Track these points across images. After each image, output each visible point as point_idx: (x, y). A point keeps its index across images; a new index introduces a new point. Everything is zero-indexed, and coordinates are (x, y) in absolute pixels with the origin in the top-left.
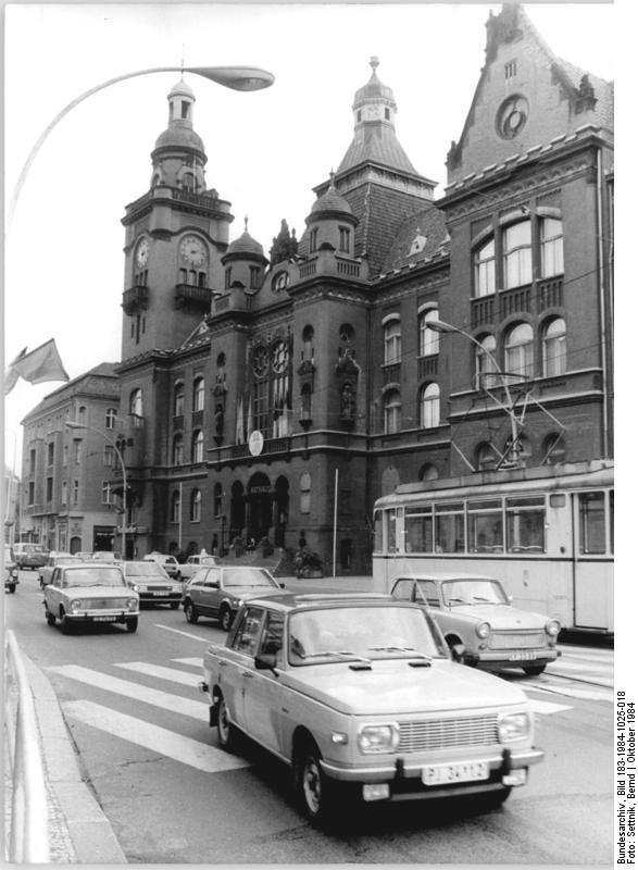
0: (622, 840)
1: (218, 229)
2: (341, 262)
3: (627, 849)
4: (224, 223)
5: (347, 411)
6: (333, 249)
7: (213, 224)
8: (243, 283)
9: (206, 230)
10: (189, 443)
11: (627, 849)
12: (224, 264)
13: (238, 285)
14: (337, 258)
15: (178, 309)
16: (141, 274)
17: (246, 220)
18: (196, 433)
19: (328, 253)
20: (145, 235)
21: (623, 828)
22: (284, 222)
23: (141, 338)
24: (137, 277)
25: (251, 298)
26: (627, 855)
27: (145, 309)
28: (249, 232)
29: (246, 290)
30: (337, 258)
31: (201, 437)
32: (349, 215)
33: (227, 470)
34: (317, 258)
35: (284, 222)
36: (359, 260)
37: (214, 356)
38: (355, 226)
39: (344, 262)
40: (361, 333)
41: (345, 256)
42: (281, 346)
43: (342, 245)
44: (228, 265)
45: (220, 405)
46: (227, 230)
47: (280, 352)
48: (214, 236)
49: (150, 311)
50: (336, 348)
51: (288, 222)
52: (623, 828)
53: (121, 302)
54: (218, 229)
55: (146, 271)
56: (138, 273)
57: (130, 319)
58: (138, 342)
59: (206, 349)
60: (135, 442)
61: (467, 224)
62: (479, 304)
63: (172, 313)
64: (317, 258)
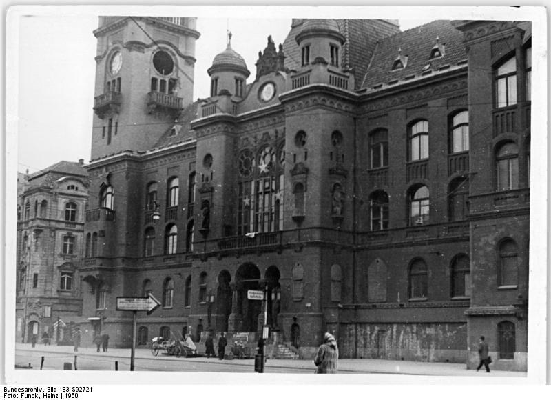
0: (19, 390)
1: (186, 44)
2: (332, 75)
3: (13, 393)
4: (191, 39)
5: (338, 209)
6: (325, 63)
7: (182, 38)
8: (231, 92)
9: (175, 44)
10: (162, 235)
11: (13, 393)
12: (210, 74)
13: (225, 93)
14: (329, 71)
15: (150, 114)
16: (114, 81)
17: (230, 35)
18: (169, 227)
19: (321, 67)
20: (120, 46)
21: (27, 390)
22: (269, 38)
23: (113, 138)
24: (109, 83)
25: (236, 106)
26: (10, 393)
27: (118, 113)
28: (233, 47)
29: (232, 98)
30: (329, 71)
31: (174, 229)
32: (336, 33)
33: (212, 260)
34: (310, 71)
35: (269, 38)
36: (348, 74)
37: (199, 156)
38: (342, 44)
39: (335, 76)
40: (347, 139)
41: (334, 69)
42: (267, 150)
43: (333, 61)
44: (215, 75)
45: (206, 201)
46: (194, 44)
47: (266, 154)
48: (182, 50)
49: (122, 115)
50: (329, 152)
51: (273, 39)
52: (27, 390)
53: (93, 106)
54: (186, 44)
55: (119, 79)
56: (110, 80)
57: (100, 122)
58: (109, 142)
59: (192, 148)
60: (106, 232)
61: (489, 42)
62: (500, 114)
63: (144, 117)
64: (310, 71)
